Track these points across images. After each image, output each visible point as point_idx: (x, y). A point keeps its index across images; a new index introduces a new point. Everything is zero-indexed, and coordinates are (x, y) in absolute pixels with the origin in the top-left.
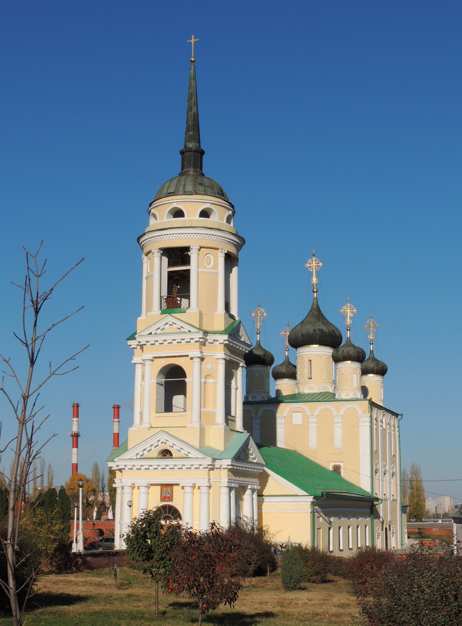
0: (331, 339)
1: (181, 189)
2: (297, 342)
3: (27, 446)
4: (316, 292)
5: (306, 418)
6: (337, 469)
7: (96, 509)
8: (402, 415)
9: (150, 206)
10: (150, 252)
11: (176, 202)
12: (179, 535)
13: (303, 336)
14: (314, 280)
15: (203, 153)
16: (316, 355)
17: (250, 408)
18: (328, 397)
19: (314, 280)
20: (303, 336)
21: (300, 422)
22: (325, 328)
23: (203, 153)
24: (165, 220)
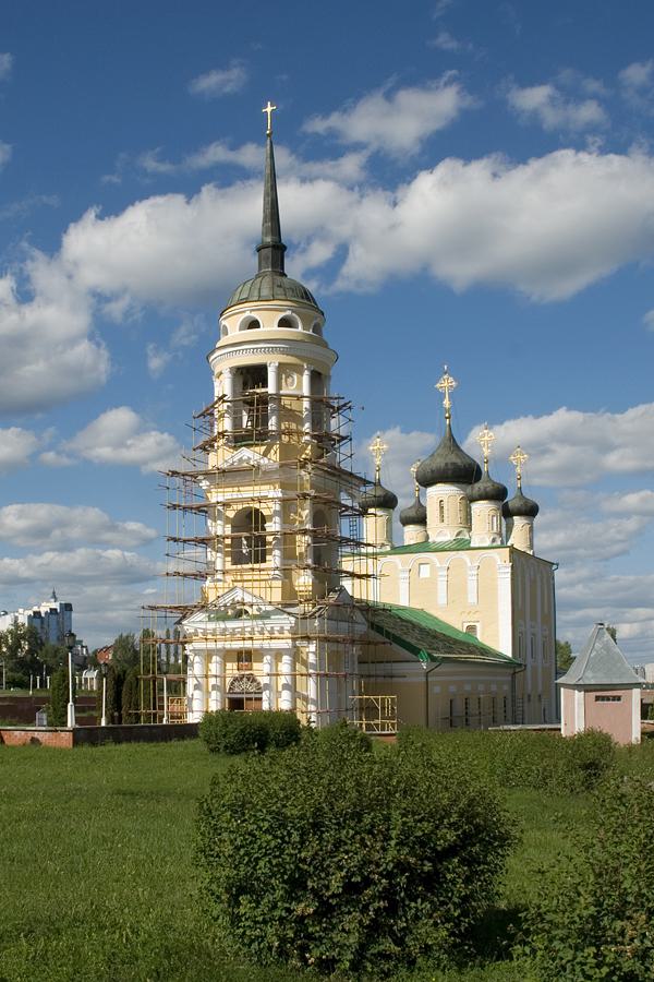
0: (465, 474)
1: (256, 293)
2: (427, 481)
3: (44, 638)
4: (449, 418)
5: (433, 570)
6: (472, 629)
7: (154, 591)
8: (557, 565)
9: (221, 315)
10: (221, 373)
11: (247, 311)
12: (101, 211)
13: (432, 471)
14: (447, 403)
15: (284, 248)
16: (442, 495)
17: (526, 721)
18: (462, 545)
19: (447, 403)
20: (432, 471)
21: (428, 575)
22: (458, 461)
23: (284, 248)
24: (238, 332)
